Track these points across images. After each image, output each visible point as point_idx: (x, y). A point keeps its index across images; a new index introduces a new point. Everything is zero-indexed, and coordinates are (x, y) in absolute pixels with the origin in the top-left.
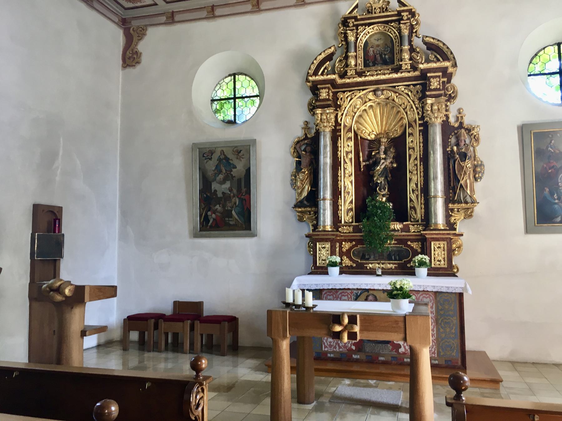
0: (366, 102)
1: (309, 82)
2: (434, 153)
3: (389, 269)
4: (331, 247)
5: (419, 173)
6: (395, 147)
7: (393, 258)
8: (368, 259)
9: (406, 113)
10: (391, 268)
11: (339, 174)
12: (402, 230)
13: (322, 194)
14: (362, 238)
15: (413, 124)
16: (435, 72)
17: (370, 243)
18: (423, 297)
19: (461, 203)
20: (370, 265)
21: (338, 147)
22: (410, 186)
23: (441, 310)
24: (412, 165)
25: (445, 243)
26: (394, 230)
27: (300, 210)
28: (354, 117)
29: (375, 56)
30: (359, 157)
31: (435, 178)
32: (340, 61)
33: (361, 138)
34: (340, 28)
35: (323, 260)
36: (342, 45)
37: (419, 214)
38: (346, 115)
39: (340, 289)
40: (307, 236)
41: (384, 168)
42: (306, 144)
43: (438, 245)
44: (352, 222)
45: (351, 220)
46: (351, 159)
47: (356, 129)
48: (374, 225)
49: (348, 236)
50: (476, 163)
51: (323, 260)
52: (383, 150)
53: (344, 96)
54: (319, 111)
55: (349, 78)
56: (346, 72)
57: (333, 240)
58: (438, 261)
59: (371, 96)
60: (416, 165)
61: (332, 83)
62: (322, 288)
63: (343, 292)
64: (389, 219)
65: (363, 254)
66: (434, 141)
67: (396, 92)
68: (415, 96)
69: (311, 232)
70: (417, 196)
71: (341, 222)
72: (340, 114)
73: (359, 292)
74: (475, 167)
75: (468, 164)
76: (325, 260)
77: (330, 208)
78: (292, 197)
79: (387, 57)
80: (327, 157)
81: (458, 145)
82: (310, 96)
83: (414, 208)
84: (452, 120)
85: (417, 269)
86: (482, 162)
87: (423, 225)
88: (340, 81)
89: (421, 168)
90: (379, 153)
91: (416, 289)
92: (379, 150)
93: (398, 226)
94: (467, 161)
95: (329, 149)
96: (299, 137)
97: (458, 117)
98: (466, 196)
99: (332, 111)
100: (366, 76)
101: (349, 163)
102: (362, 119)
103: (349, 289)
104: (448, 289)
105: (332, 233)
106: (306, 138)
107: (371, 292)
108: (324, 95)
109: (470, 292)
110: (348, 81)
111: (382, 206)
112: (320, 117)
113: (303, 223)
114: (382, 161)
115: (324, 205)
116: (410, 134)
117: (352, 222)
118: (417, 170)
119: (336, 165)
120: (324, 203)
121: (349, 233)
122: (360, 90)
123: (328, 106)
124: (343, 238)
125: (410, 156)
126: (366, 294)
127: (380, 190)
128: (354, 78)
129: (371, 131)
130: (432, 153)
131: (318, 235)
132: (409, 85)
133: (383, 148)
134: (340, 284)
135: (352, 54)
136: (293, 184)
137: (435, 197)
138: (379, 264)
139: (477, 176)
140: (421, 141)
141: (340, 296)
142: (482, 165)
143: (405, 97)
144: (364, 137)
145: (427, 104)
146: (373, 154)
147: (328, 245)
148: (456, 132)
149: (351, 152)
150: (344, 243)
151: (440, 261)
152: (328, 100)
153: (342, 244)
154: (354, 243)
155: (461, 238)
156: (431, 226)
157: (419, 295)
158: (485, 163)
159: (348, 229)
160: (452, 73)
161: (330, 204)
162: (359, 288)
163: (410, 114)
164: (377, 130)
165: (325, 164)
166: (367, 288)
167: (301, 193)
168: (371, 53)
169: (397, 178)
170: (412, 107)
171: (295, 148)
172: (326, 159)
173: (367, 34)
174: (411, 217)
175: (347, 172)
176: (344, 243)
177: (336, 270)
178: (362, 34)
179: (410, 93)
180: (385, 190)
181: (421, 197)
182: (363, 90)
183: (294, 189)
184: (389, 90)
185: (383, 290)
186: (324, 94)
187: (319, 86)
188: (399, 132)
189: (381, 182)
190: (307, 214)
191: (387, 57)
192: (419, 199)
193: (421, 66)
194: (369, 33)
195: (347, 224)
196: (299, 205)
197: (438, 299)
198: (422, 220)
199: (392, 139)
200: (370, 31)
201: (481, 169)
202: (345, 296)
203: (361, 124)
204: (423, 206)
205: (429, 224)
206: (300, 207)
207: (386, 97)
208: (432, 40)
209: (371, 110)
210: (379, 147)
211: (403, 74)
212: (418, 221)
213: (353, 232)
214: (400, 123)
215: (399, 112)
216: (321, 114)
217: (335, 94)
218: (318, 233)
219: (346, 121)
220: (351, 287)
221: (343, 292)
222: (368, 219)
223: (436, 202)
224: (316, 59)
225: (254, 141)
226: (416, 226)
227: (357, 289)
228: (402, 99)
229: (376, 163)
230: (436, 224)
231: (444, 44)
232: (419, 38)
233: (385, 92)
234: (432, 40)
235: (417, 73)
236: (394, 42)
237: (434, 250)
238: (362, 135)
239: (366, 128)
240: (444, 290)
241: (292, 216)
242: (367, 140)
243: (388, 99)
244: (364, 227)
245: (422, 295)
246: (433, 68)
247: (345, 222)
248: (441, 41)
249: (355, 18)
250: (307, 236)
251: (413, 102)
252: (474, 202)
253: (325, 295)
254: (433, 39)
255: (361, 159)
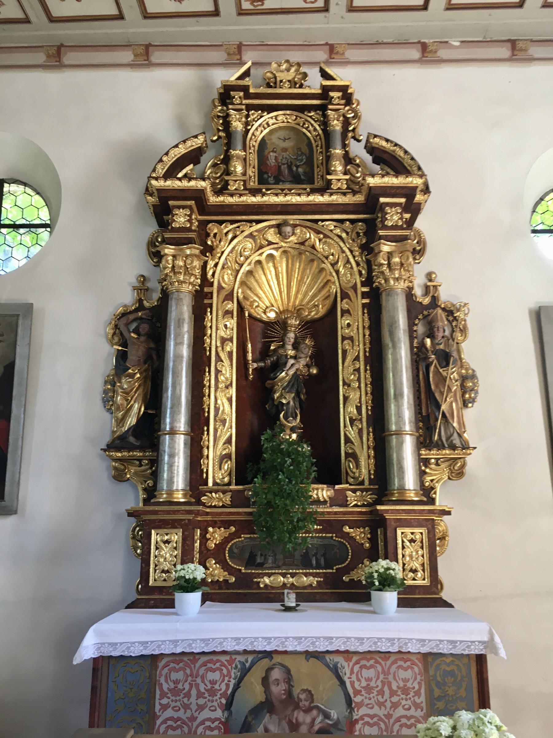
0: (261, 247)
1: (151, 195)
2: (394, 347)
3: (305, 588)
4: (184, 539)
5: (363, 385)
6: (314, 337)
7: (314, 562)
8: (261, 566)
9: (337, 272)
10: (311, 585)
11: (206, 383)
12: (333, 501)
13: (168, 420)
14: (250, 518)
15: (351, 293)
16: (393, 196)
17: (270, 532)
18: (399, 667)
19: (444, 448)
20: (267, 580)
21: (205, 327)
22: (347, 412)
23: (439, 699)
24: (351, 371)
25: (423, 530)
26: (318, 502)
27: (119, 455)
28: (238, 271)
29: (279, 167)
30: (245, 352)
31: (398, 395)
32: (214, 165)
33: (250, 315)
34: (216, 107)
35: (163, 571)
36: (220, 137)
37: (365, 469)
38: (223, 268)
39: (203, 653)
40: (131, 514)
41: (293, 375)
42: (141, 318)
43: (410, 536)
44: (229, 484)
45: (226, 480)
46: (230, 354)
47: (241, 296)
48: (277, 490)
49: (221, 514)
50: (463, 371)
51: (163, 571)
52: (292, 340)
53: (220, 231)
54: (169, 250)
55: (232, 195)
56: (227, 183)
57: (188, 521)
58: (412, 570)
59: (271, 235)
60: (358, 370)
61: (198, 196)
62: (157, 652)
63: (210, 661)
64: (308, 478)
65: (251, 553)
66: (393, 324)
67: (318, 232)
68: (353, 240)
69: (141, 504)
70: (360, 431)
71: (206, 484)
72: (211, 264)
73: (250, 660)
74: (464, 379)
75: (453, 374)
76: (168, 572)
77: (185, 453)
78: (103, 426)
79: (300, 170)
80: (182, 343)
81: (431, 335)
82: (152, 227)
83: (353, 456)
84: (418, 292)
85: (375, 594)
86: (474, 371)
87: (374, 492)
88: (213, 199)
89: (366, 376)
90: (283, 346)
91: (383, 649)
92: (283, 340)
93: (323, 492)
94: (451, 366)
95: (187, 328)
96: (125, 306)
97: (427, 288)
98: (452, 435)
99: (197, 252)
100: (264, 195)
101: (226, 362)
102: (252, 280)
103: (224, 652)
104: (455, 647)
105: (187, 508)
106: (141, 307)
107: (277, 659)
108: (182, 220)
109: (502, 653)
110: (230, 200)
111: (290, 451)
112: (170, 262)
113: (125, 485)
114: (291, 361)
115: (172, 446)
116: (345, 312)
117: (229, 484)
118: (359, 380)
119: (200, 362)
120: (172, 440)
121: (223, 506)
122: (251, 221)
123: (189, 241)
124: (209, 518)
125: (344, 352)
126: (265, 663)
127: (286, 417)
128: (241, 195)
129: (268, 304)
130: (390, 345)
131: (156, 512)
132: (342, 221)
133: (291, 336)
134: (203, 640)
135: (237, 152)
136: (108, 400)
137: (399, 433)
138: (284, 575)
139: (467, 396)
140: (367, 324)
141: (202, 671)
142: (473, 377)
143: (338, 248)
144: (255, 314)
145: (380, 252)
146: (272, 348)
147: (176, 537)
148: (425, 313)
149: (231, 340)
150: (211, 529)
151: (414, 571)
152: (189, 230)
153: (207, 532)
154: (233, 529)
155: (445, 518)
156: (393, 494)
157: (388, 663)
158: (478, 374)
159: (220, 499)
160: (420, 204)
161: (185, 444)
162: (250, 648)
163: (345, 274)
164: (280, 305)
165: (178, 357)
166: (268, 649)
167: (121, 421)
168: (272, 161)
169: (319, 395)
170: (348, 262)
171: (116, 326)
172: (179, 349)
173: (264, 125)
174: (347, 473)
175: (221, 378)
176: (211, 529)
177: (194, 598)
178: (256, 125)
179: (344, 235)
180: (295, 418)
181: (368, 434)
182: (258, 222)
183: (109, 410)
184: (306, 227)
185: (307, 652)
186: (180, 219)
187: (171, 203)
188: (322, 311)
189: (288, 403)
190: (133, 465)
191: (300, 170)
192: (365, 439)
193: (372, 181)
194: (269, 126)
195: (219, 487)
196: (117, 443)
197: (432, 672)
198: (371, 482)
199: (307, 322)
200: (271, 122)
201: (473, 383)
202: (214, 671)
203: (250, 289)
204: (372, 453)
205: (386, 489)
206: (119, 450)
207: (300, 240)
208: (384, 143)
209: (271, 264)
210: (285, 335)
211: (334, 197)
212: (362, 483)
213: (232, 506)
214: (324, 292)
215: (322, 270)
216: (174, 256)
217: (203, 224)
218: (157, 508)
219: (222, 277)
220: (229, 649)
221: (210, 661)
222: (263, 478)
223: (401, 444)
224: (167, 154)
225: (28, 308)
226: (358, 493)
227: (245, 652)
228: (329, 245)
229: (278, 365)
230: (402, 489)
231: (406, 152)
232: (359, 141)
233: (298, 231)
234: (384, 143)
235: (360, 198)
236: (314, 145)
237: (403, 548)
238: (252, 311)
239: (259, 298)
240: (445, 649)
241: (101, 467)
242: (260, 321)
243: (302, 243)
244: (256, 494)
245: (395, 662)
246: (392, 188)
247: (215, 483)
248: (401, 147)
249: (245, 89)
250: (131, 514)
251: (351, 252)
252: (465, 446)
253: (166, 670)
254: (387, 140)
255: (250, 356)
